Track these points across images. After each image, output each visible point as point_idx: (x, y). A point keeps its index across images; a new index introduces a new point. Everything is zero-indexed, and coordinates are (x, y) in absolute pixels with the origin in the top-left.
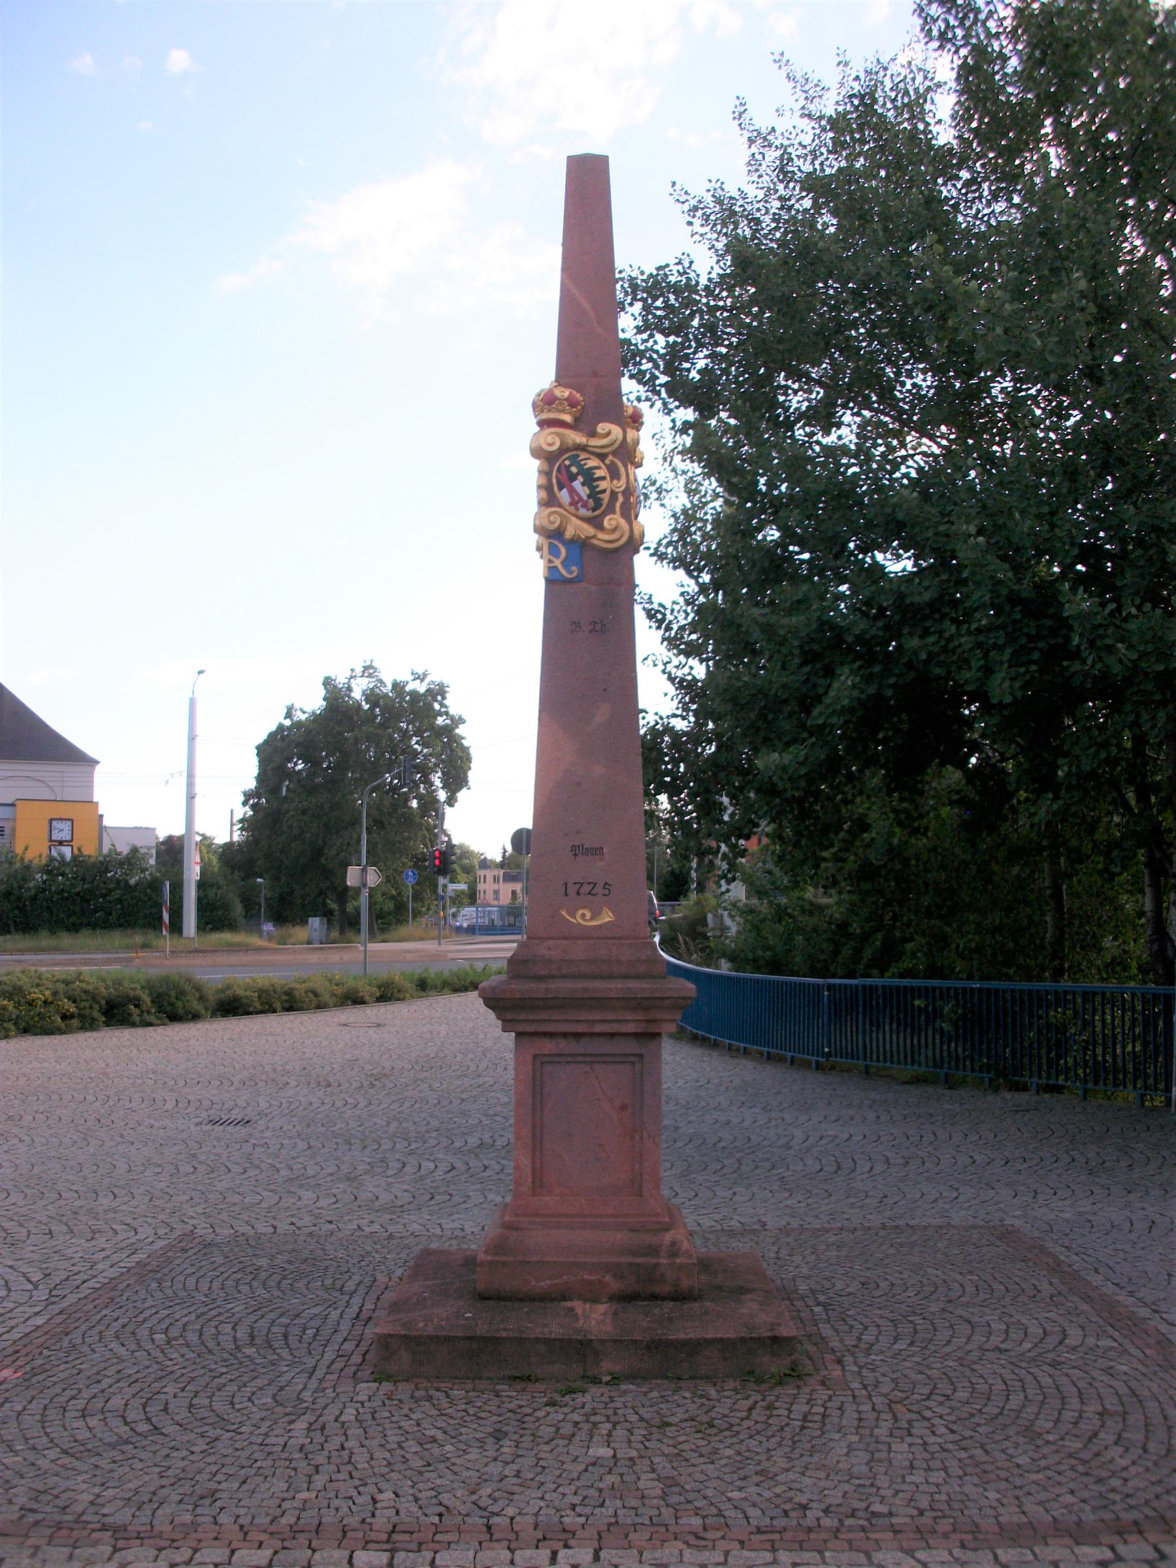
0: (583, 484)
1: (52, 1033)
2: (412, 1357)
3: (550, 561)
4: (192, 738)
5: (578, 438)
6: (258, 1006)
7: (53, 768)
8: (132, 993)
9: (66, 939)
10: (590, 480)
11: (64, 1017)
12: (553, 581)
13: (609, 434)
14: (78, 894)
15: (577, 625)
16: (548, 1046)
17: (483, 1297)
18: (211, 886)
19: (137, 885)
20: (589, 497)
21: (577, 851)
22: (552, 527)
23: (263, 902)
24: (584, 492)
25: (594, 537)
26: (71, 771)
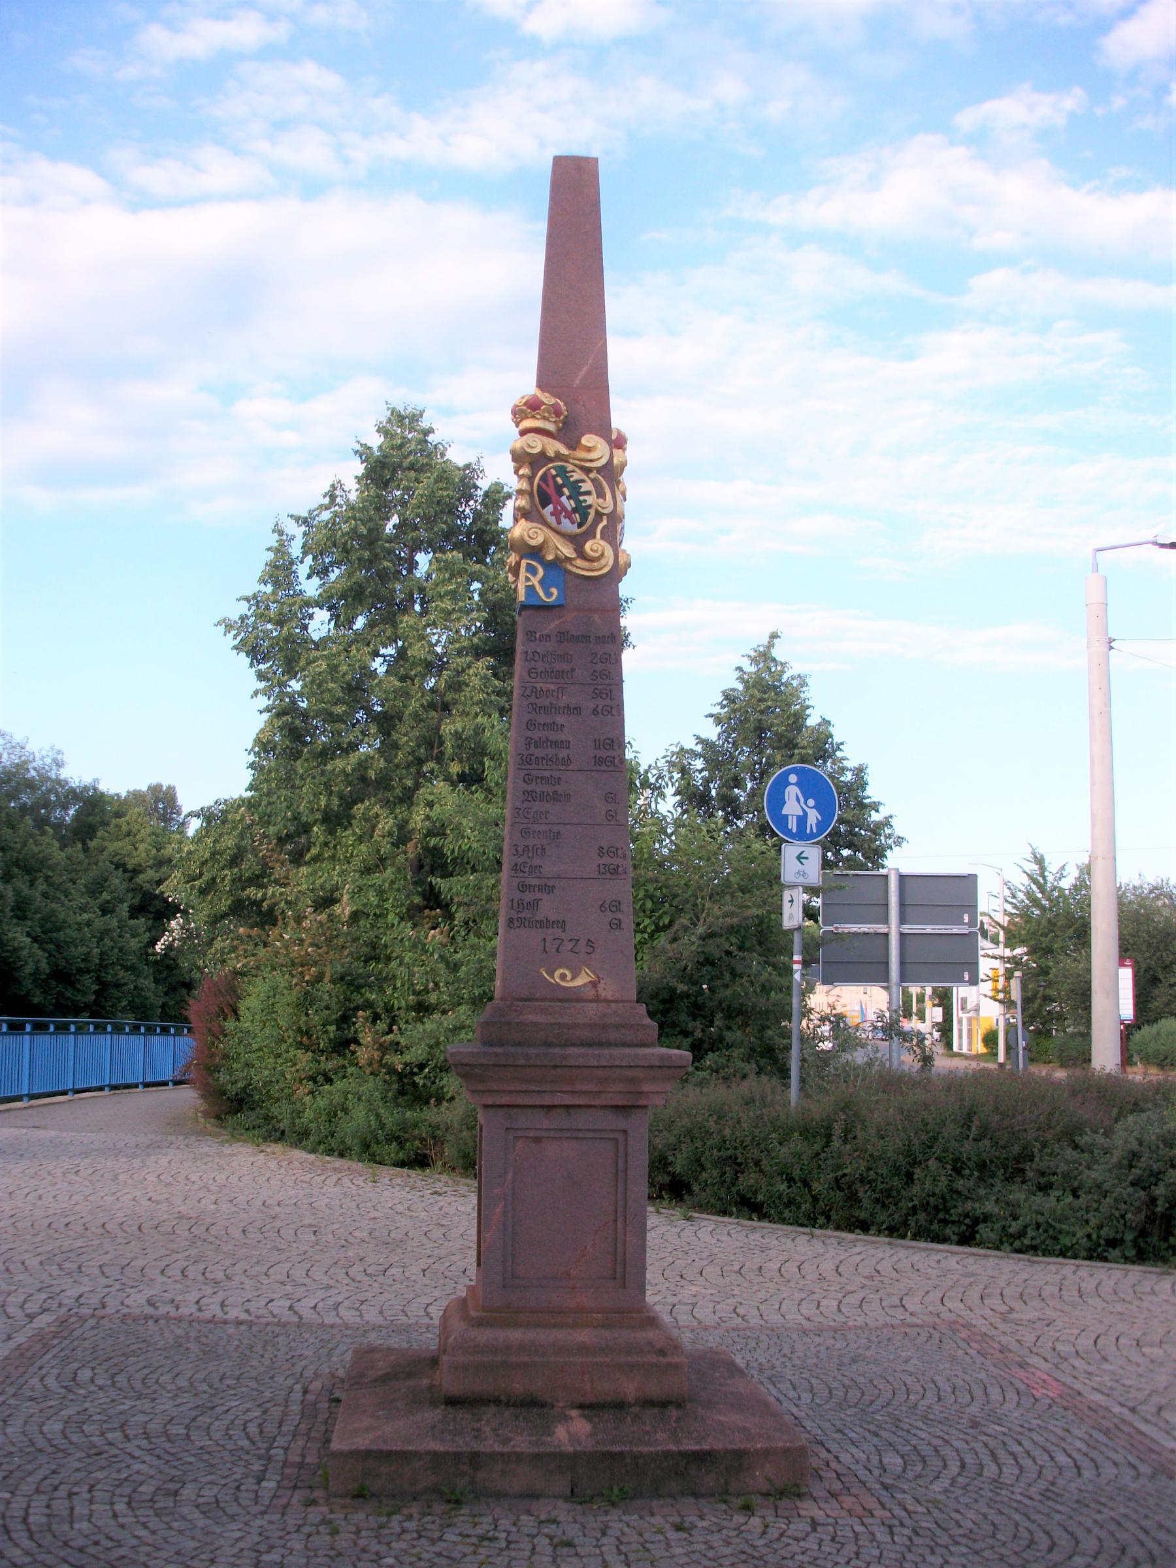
2: (372, 1484)
17: (453, 1402)
22: (533, 543)
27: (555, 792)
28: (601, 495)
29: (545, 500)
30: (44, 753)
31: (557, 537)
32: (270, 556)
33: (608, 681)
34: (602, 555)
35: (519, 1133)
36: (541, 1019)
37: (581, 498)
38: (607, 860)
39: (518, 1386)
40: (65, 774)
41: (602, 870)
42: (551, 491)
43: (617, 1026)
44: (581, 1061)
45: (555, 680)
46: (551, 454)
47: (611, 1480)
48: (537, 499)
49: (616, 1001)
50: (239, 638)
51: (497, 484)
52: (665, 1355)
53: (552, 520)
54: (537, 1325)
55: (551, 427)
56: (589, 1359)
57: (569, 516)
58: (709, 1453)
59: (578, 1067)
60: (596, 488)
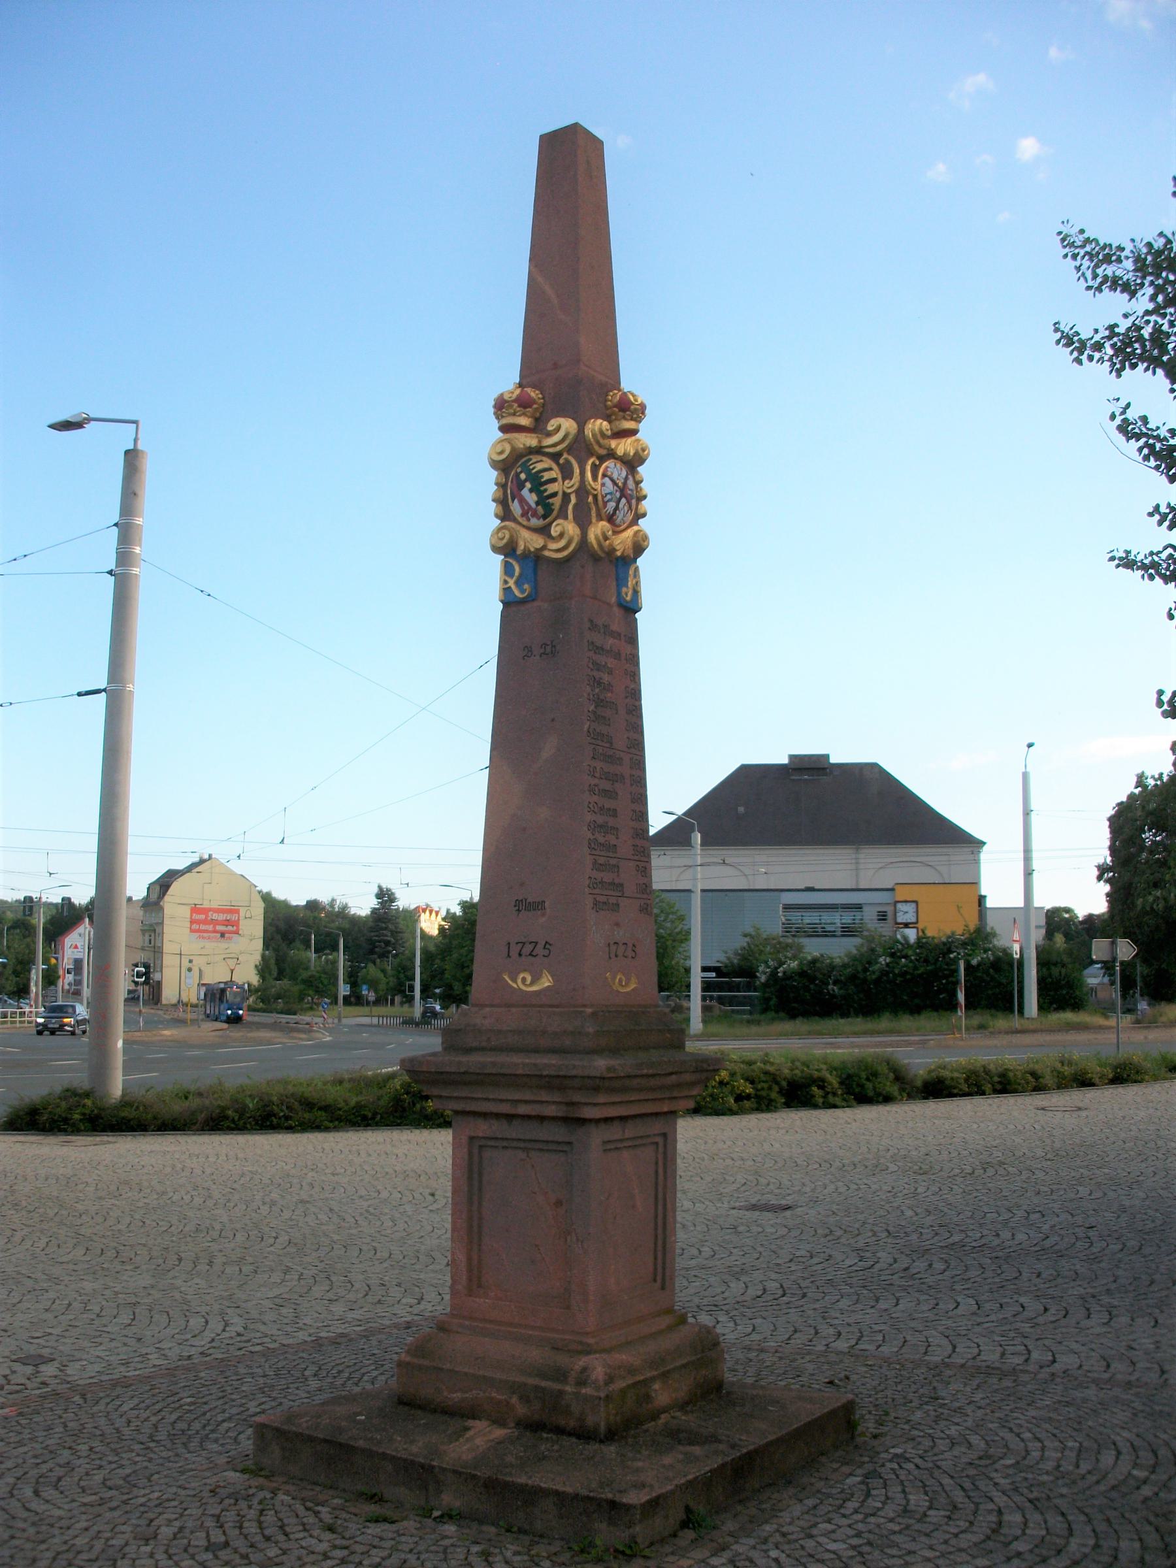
0: (531, 491)
1: (723, 1114)
3: (506, 582)
4: (1027, 813)
5: (531, 441)
6: (965, 1088)
7: (826, 851)
8: (816, 1074)
9: (906, 1021)
10: (538, 484)
11: (739, 1098)
12: (510, 604)
13: (558, 429)
14: (920, 976)
15: (528, 650)
16: (483, 1128)
18: (1055, 964)
19: (979, 965)
20: (537, 503)
21: (522, 905)
23: (1138, 979)
24: (531, 499)
25: (544, 547)
26: (959, 854)
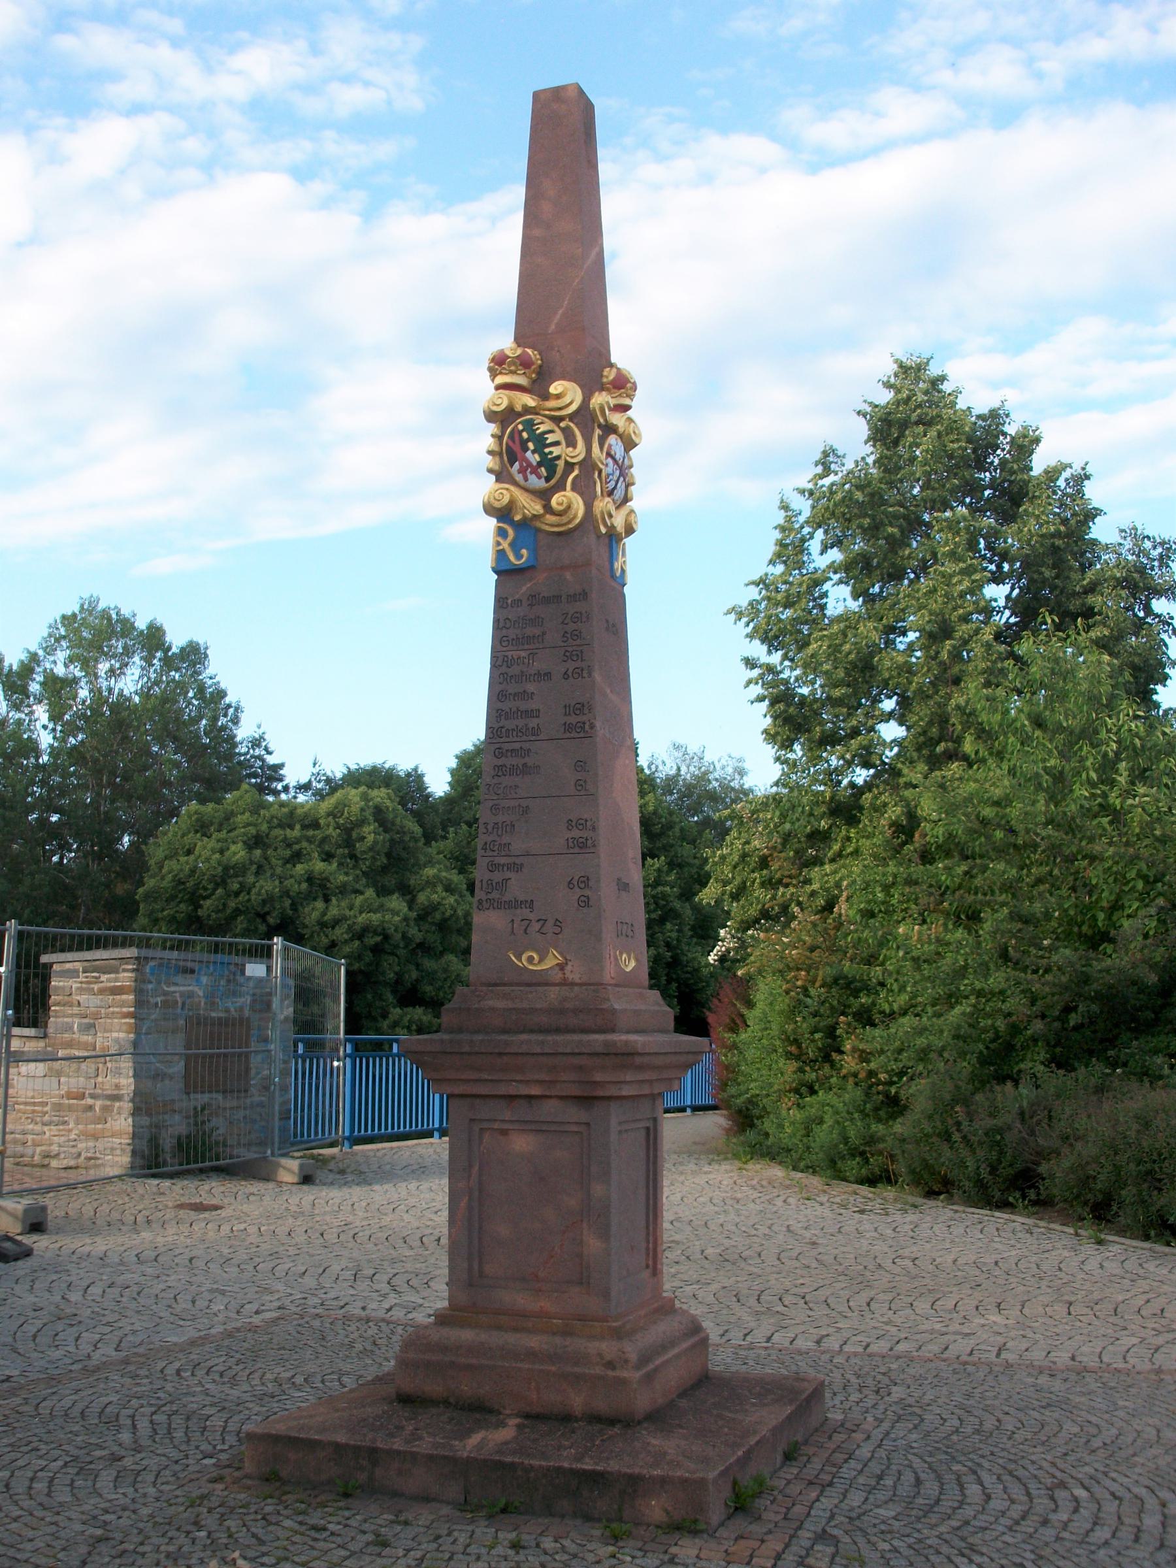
0: (534, 452)
3: (498, 544)
27: (525, 765)
28: (571, 443)
29: (512, 459)
30: (723, 762)
31: (526, 494)
32: (777, 535)
33: (578, 642)
34: (569, 507)
35: (485, 1125)
36: (500, 1004)
37: (547, 450)
38: (576, 833)
39: (467, 1388)
40: (748, 782)
41: (571, 844)
42: (517, 448)
43: (576, 1011)
44: (524, 1049)
45: (526, 647)
46: (519, 408)
47: (504, 1495)
48: (505, 458)
49: (581, 985)
50: (751, 625)
51: (1025, 428)
52: (614, 1368)
53: (519, 478)
54: (499, 1328)
55: (521, 380)
56: (537, 1366)
57: (535, 471)
58: (601, 1474)
59: (533, 1054)
60: (566, 438)
